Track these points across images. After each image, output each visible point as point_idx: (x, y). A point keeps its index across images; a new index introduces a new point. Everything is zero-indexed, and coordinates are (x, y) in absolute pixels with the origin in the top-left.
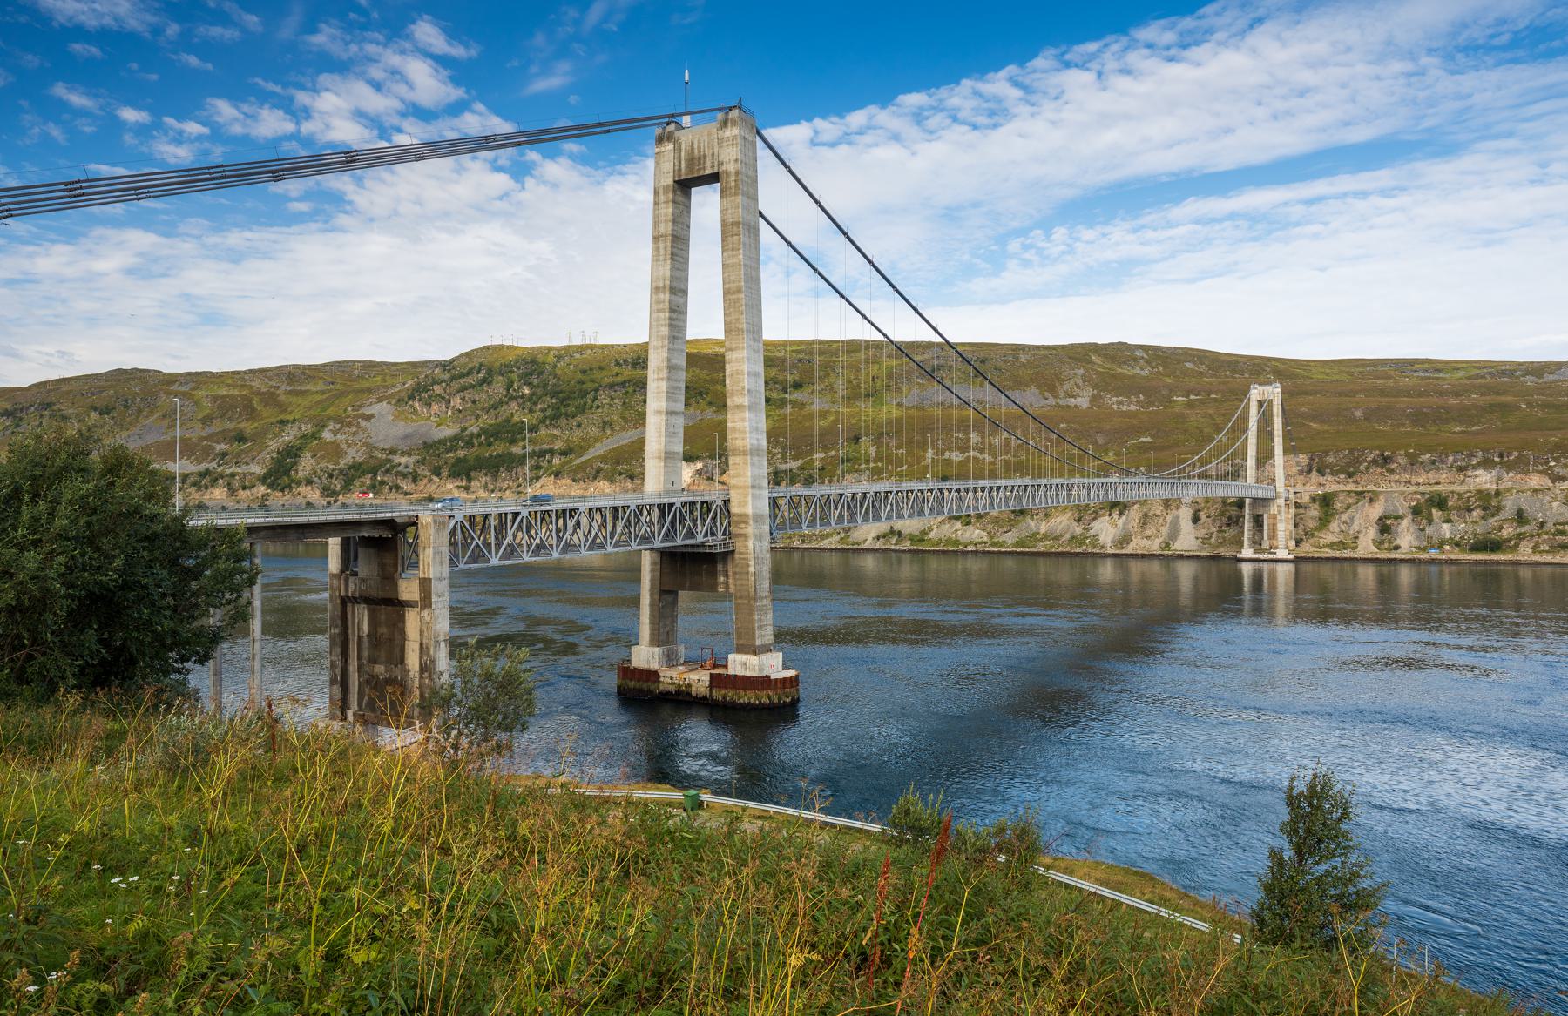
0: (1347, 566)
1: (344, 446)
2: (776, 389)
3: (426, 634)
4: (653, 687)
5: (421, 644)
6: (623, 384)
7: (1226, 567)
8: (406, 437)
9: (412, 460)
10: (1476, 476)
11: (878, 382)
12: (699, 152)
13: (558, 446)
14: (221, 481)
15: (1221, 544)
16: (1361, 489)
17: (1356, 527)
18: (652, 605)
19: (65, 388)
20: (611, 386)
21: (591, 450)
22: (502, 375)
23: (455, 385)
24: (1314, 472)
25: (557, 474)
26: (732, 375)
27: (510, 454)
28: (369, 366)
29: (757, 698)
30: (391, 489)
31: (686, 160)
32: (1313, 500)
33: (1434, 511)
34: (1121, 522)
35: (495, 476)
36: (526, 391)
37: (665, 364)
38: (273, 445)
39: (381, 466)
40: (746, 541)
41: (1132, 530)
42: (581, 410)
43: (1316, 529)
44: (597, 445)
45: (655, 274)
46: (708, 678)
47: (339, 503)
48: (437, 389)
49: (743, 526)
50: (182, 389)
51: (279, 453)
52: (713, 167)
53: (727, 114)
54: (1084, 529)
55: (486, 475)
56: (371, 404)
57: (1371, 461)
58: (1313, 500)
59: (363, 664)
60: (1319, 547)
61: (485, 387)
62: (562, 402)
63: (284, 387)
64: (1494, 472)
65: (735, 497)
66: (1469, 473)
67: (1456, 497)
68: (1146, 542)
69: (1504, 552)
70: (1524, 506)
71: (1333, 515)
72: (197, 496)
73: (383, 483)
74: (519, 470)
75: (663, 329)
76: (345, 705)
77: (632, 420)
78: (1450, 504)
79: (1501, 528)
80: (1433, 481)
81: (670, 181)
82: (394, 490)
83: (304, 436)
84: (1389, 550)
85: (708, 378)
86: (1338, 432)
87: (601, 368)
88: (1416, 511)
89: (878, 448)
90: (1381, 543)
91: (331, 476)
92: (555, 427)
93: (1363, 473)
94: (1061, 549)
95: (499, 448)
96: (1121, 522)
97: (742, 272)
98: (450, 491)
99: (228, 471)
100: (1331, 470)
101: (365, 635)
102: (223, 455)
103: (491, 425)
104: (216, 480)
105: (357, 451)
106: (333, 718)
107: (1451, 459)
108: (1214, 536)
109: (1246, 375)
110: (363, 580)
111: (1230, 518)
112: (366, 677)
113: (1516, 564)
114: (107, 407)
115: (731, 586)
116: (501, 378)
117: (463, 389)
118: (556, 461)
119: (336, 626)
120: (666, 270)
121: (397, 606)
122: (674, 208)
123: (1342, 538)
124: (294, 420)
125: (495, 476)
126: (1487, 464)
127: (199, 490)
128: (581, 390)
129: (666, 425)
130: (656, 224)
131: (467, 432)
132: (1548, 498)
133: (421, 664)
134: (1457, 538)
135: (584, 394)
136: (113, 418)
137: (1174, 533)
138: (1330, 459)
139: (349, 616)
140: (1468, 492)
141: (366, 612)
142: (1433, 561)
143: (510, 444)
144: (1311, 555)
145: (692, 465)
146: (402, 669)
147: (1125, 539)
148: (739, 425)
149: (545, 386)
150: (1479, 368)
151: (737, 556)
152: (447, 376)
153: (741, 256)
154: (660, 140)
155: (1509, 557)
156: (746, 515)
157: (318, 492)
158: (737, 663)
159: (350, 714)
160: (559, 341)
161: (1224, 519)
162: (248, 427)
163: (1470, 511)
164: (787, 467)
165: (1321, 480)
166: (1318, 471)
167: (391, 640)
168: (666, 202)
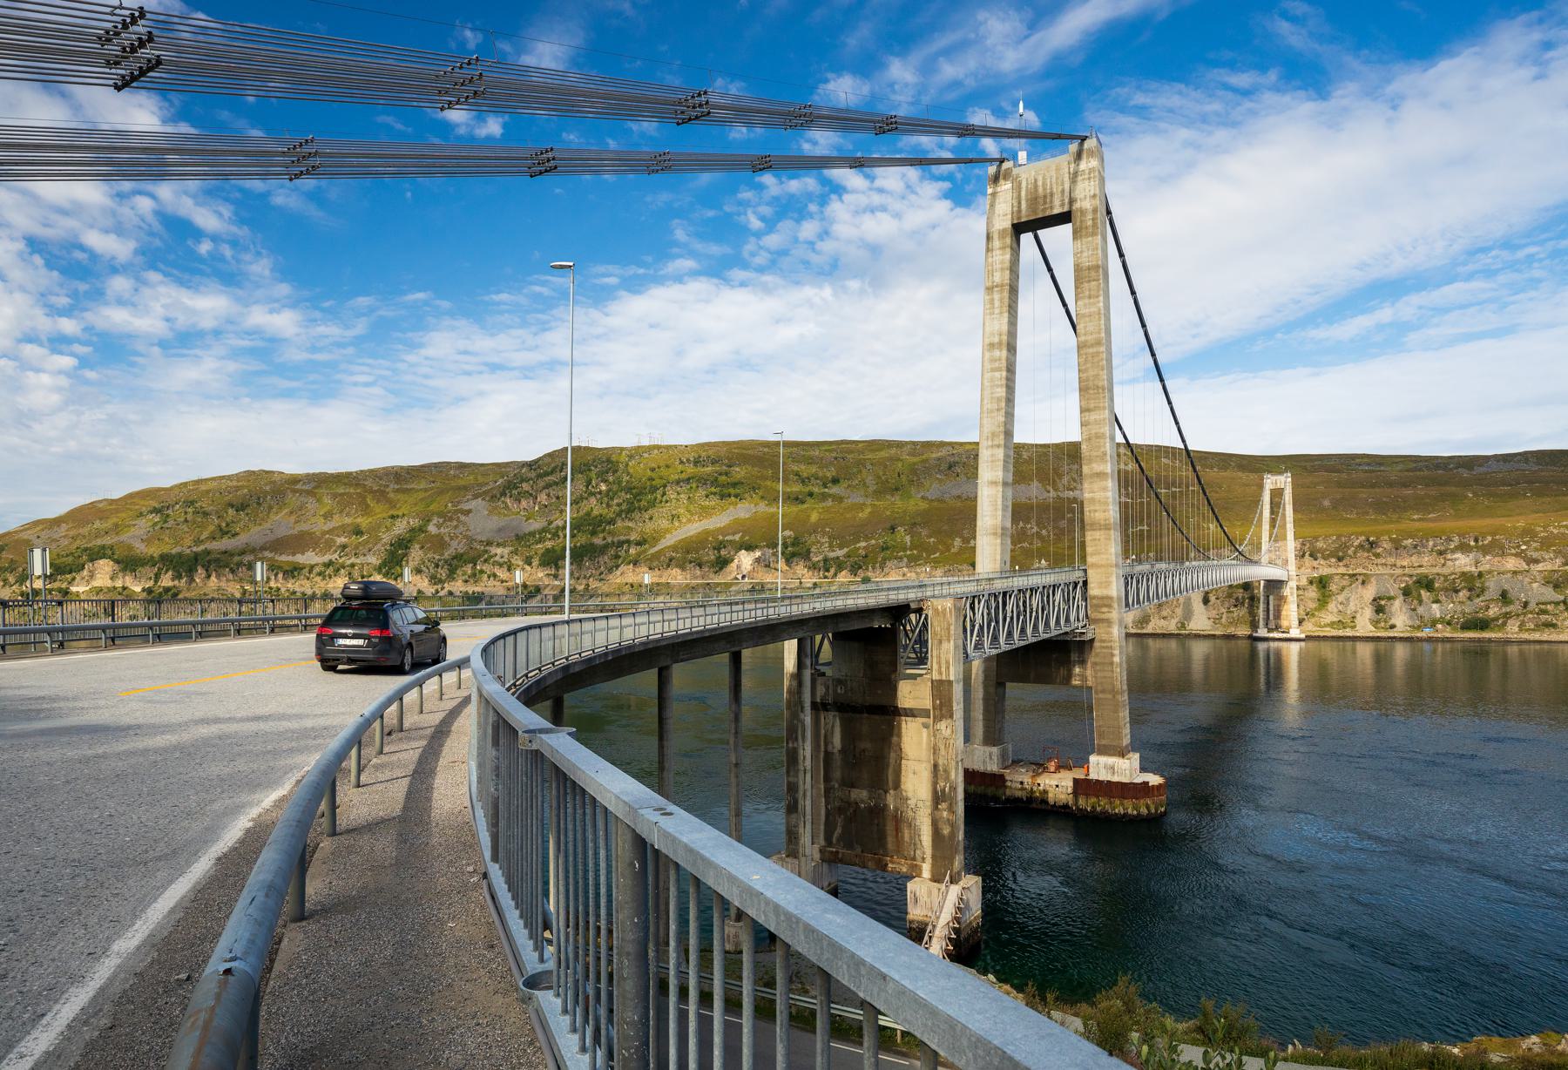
0: (1349, 644)
1: (447, 539)
3: (943, 752)
5: (935, 766)
8: (500, 530)
9: (506, 551)
10: (1456, 559)
11: (904, 478)
12: (1045, 189)
13: (634, 536)
14: (342, 571)
16: (1351, 572)
17: (1352, 607)
18: (986, 699)
19: (203, 488)
20: (678, 482)
21: (663, 541)
23: (541, 483)
25: (636, 563)
27: (592, 544)
28: (462, 466)
29: (1134, 808)
30: (489, 577)
32: (1311, 583)
33: (1422, 592)
36: (603, 487)
37: (1002, 429)
38: (386, 538)
39: (479, 556)
40: (1109, 627)
42: (652, 504)
43: (1316, 609)
47: (446, 590)
48: (526, 486)
50: (306, 487)
51: (392, 545)
52: (1062, 205)
56: (468, 500)
57: (1357, 547)
59: (833, 788)
62: (635, 498)
63: (393, 486)
64: (1471, 556)
66: (1449, 556)
67: (1442, 578)
69: (1492, 630)
70: (1506, 587)
71: (1330, 596)
72: (322, 584)
73: (482, 572)
74: (600, 559)
75: (999, 390)
78: (1437, 585)
79: (1488, 608)
80: (1416, 565)
81: (1007, 224)
82: (492, 578)
83: (412, 530)
84: (1385, 629)
88: (1406, 592)
90: (1378, 622)
91: (437, 566)
92: (630, 520)
98: (541, 579)
99: (349, 562)
100: (1322, 554)
101: (835, 751)
102: (344, 547)
104: (338, 570)
105: (459, 543)
107: (1431, 543)
108: (1224, 616)
109: (1215, 470)
110: (839, 682)
111: (1237, 599)
113: (1508, 642)
114: (242, 504)
116: (580, 476)
117: (547, 486)
120: (1002, 324)
121: (888, 713)
123: (1340, 618)
124: (404, 515)
126: (1463, 548)
127: (324, 579)
128: (651, 486)
131: (553, 525)
132: (1527, 580)
133: (935, 792)
134: (1448, 617)
135: (654, 489)
136: (247, 514)
137: (1188, 614)
140: (1453, 574)
142: (1430, 640)
144: (1316, 634)
145: (752, 554)
146: (896, 796)
148: (1098, 495)
149: (620, 483)
150: (1415, 462)
151: (1097, 644)
152: (533, 474)
155: (1500, 635)
156: (1111, 598)
157: (426, 580)
158: (1102, 765)
162: (363, 522)
163: (1457, 591)
164: (832, 555)
165: (1315, 563)
166: (1311, 555)
168: (1003, 248)
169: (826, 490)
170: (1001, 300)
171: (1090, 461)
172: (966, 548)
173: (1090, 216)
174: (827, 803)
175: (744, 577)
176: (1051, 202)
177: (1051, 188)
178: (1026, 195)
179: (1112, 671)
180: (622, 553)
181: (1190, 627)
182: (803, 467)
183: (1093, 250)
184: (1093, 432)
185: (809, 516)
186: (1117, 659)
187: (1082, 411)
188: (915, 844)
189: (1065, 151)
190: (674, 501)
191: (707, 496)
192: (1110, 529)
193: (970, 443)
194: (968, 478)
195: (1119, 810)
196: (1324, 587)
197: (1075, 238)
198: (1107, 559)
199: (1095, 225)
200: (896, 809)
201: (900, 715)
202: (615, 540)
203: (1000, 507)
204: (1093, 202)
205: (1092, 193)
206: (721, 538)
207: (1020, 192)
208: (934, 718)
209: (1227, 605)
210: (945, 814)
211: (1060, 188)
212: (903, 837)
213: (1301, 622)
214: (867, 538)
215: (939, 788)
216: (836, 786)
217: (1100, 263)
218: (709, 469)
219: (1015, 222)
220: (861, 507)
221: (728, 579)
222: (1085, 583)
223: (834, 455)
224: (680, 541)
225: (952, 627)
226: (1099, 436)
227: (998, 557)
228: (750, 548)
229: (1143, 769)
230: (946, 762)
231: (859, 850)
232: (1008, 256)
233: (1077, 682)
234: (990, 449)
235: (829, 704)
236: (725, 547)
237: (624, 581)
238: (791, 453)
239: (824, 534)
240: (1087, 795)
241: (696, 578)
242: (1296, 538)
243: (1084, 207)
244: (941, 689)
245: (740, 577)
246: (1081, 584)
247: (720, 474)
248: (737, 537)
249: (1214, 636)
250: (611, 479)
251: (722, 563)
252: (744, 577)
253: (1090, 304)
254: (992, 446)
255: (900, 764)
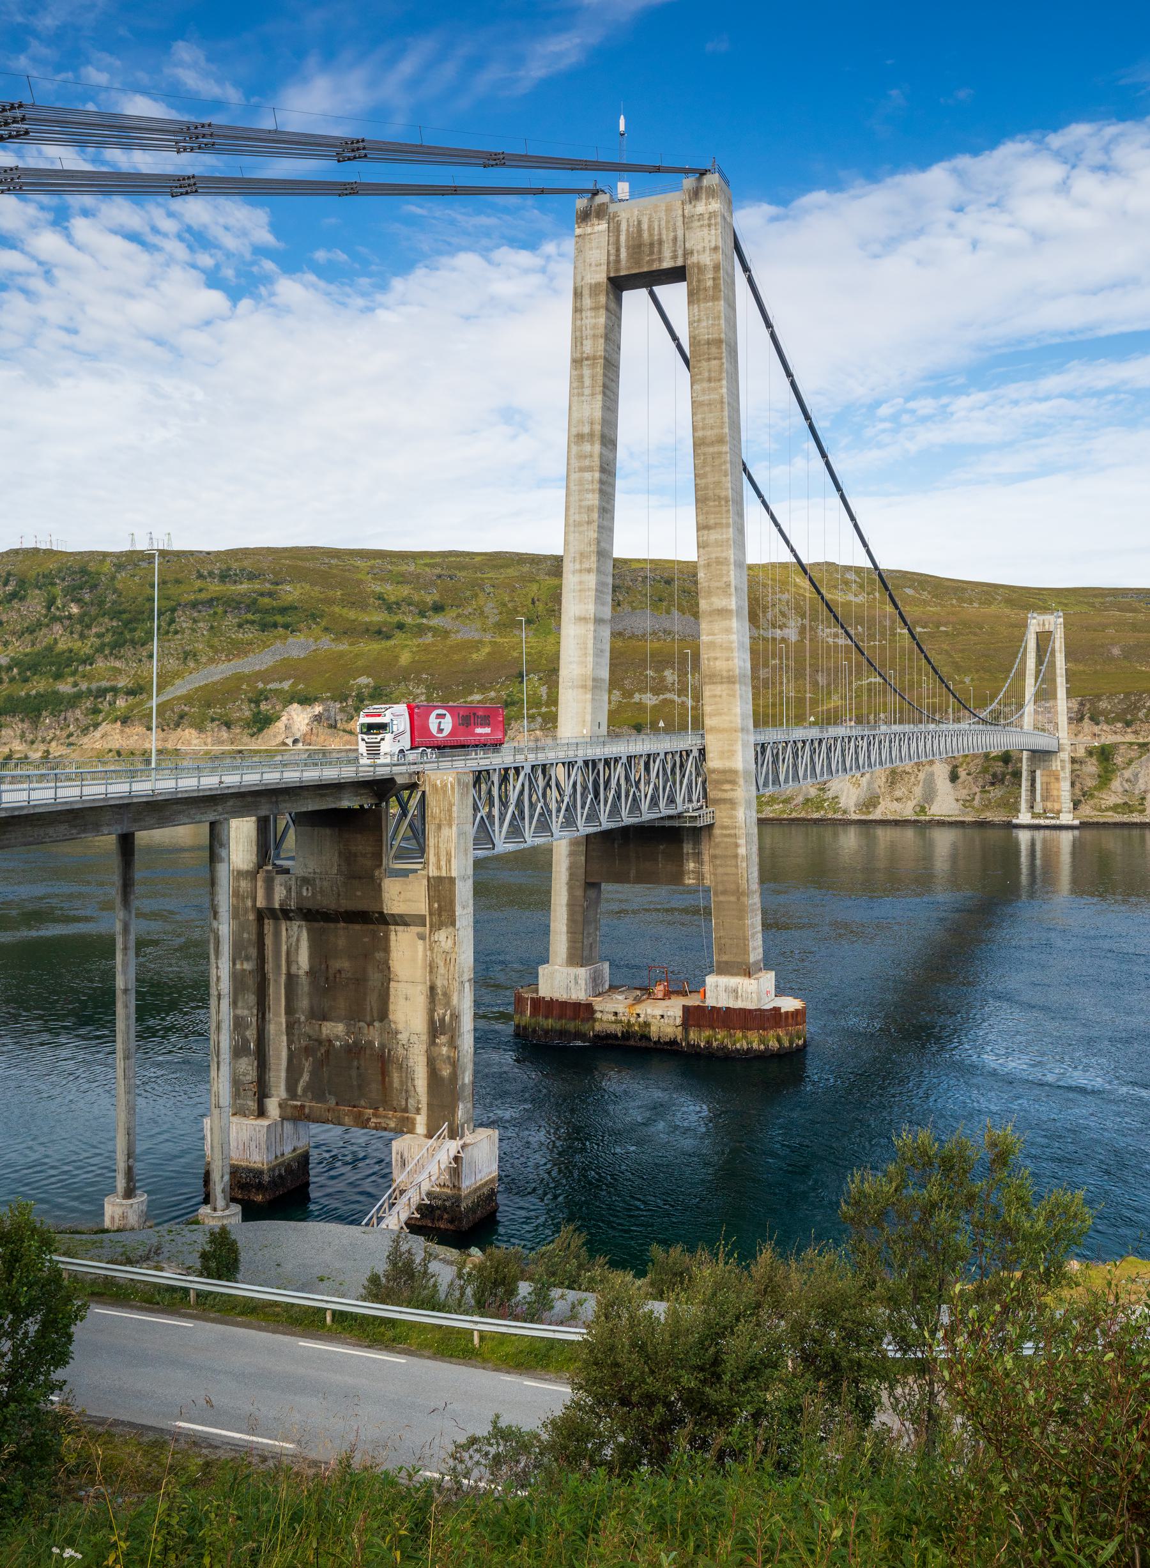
0: (1136, 832)
2: (410, 612)
4: (585, 1028)
5: (432, 988)
6: (210, 602)
7: (993, 835)
12: (651, 235)
13: (122, 682)
15: (986, 807)
16: (1141, 740)
18: (571, 905)
20: (194, 605)
22: (40, 589)
24: (1086, 720)
25: (125, 720)
26: (709, 565)
27: (56, 693)
29: (761, 1041)
31: (628, 248)
32: (1090, 753)
34: (864, 781)
35: (35, 723)
36: (75, 609)
37: (594, 548)
40: (733, 809)
41: (878, 790)
43: (1095, 788)
44: (177, 682)
45: (575, 415)
46: (680, 1013)
49: (727, 787)
52: (675, 257)
53: (699, 180)
54: (820, 789)
55: (22, 721)
58: (1090, 753)
59: (298, 1021)
60: (1101, 810)
61: (15, 604)
65: (713, 743)
68: (896, 806)
71: (1113, 771)
74: (69, 714)
75: (590, 496)
76: (262, 1093)
77: (223, 651)
81: (601, 277)
85: (322, 596)
86: (1096, 672)
87: (178, 582)
89: (549, 688)
93: (1142, 721)
94: (794, 815)
95: (39, 685)
96: (864, 781)
97: (726, 413)
100: (1106, 718)
101: (301, 972)
103: (26, 655)
106: (240, 1112)
108: (977, 797)
109: (975, 605)
110: (305, 881)
111: (994, 775)
112: (303, 1043)
115: (707, 876)
116: (37, 592)
118: (121, 703)
119: (247, 958)
120: (594, 409)
122: (607, 318)
123: (1126, 799)
125: (35, 723)
129: (595, 638)
130: (578, 340)
133: (431, 1022)
137: (930, 795)
138: (1103, 705)
139: (269, 941)
141: (305, 935)
143: (55, 679)
144: (1095, 820)
145: (309, 709)
146: (382, 1031)
147: (871, 802)
148: (719, 638)
149: (101, 604)
151: (717, 831)
153: (724, 390)
154: (584, 216)
156: (735, 772)
158: (721, 989)
159: (273, 1106)
160: (118, 544)
161: (988, 777)
165: (1096, 729)
166: (1092, 719)
167: (360, 981)
168: (595, 309)
169: (424, 621)
170: (593, 377)
171: (709, 593)
172: (628, 704)
173: (710, 275)
174: (290, 1042)
175: (295, 742)
176: (660, 252)
177: (660, 234)
178: (627, 240)
179: (736, 866)
180: (105, 706)
181: (931, 812)
182: (389, 588)
183: (714, 319)
184: (714, 556)
185: (397, 657)
186: (742, 851)
187: (700, 528)
188: (407, 1091)
189: (678, 188)
190: (188, 632)
191: (240, 626)
192: (734, 683)
193: (638, 561)
194: (634, 609)
195: (741, 1045)
196: (1107, 759)
197: (690, 302)
198: (731, 722)
199: (716, 287)
200: (383, 1046)
201: (387, 923)
202: (94, 686)
203: (591, 651)
204: (715, 256)
205: (713, 245)
206: (260, 685)
207: (618, 236)
208: (431, 926)
209: (981, 782)
210: (444, 1050)
211: (672, 235)
212: (391, 1083)
213: (1076, 804)
214: (483, 689)
215: (436, 1017)
216: (303, 1018)
217: (723, 336)
218: (244, 587)
219: (612, 275)
220: (476, 645)
221: (272, 744)
222: (702, 752)
223: (438, 571)
224: (197, 690)
225: (455, 809)
226: (720, 562)
227: (588, 718)
228: (305, 701)
229: (780, 991)
230: (446, 983)
231: (332, 1102)
232: (602, 320)
233: (691, 881)
234: (577, 575)
235: (292, 911)
236: (266, 699)
237: (109, 746)
238: (372, 567)
239: (419, 682)
240: (699, 1026)
241: (222, 743)
242: (1070, 694)
243: (702, 263)
244: (441, 889)
245: (289, 741)
246: (695, 753)
247: (262, 595)
248: (286, 685)
249: (963, 823)
250: (87, 598)
251: (262, 722)
252: (295, 742)
253: (709, 389)
254: (581, 571)
255: (388, 988)
